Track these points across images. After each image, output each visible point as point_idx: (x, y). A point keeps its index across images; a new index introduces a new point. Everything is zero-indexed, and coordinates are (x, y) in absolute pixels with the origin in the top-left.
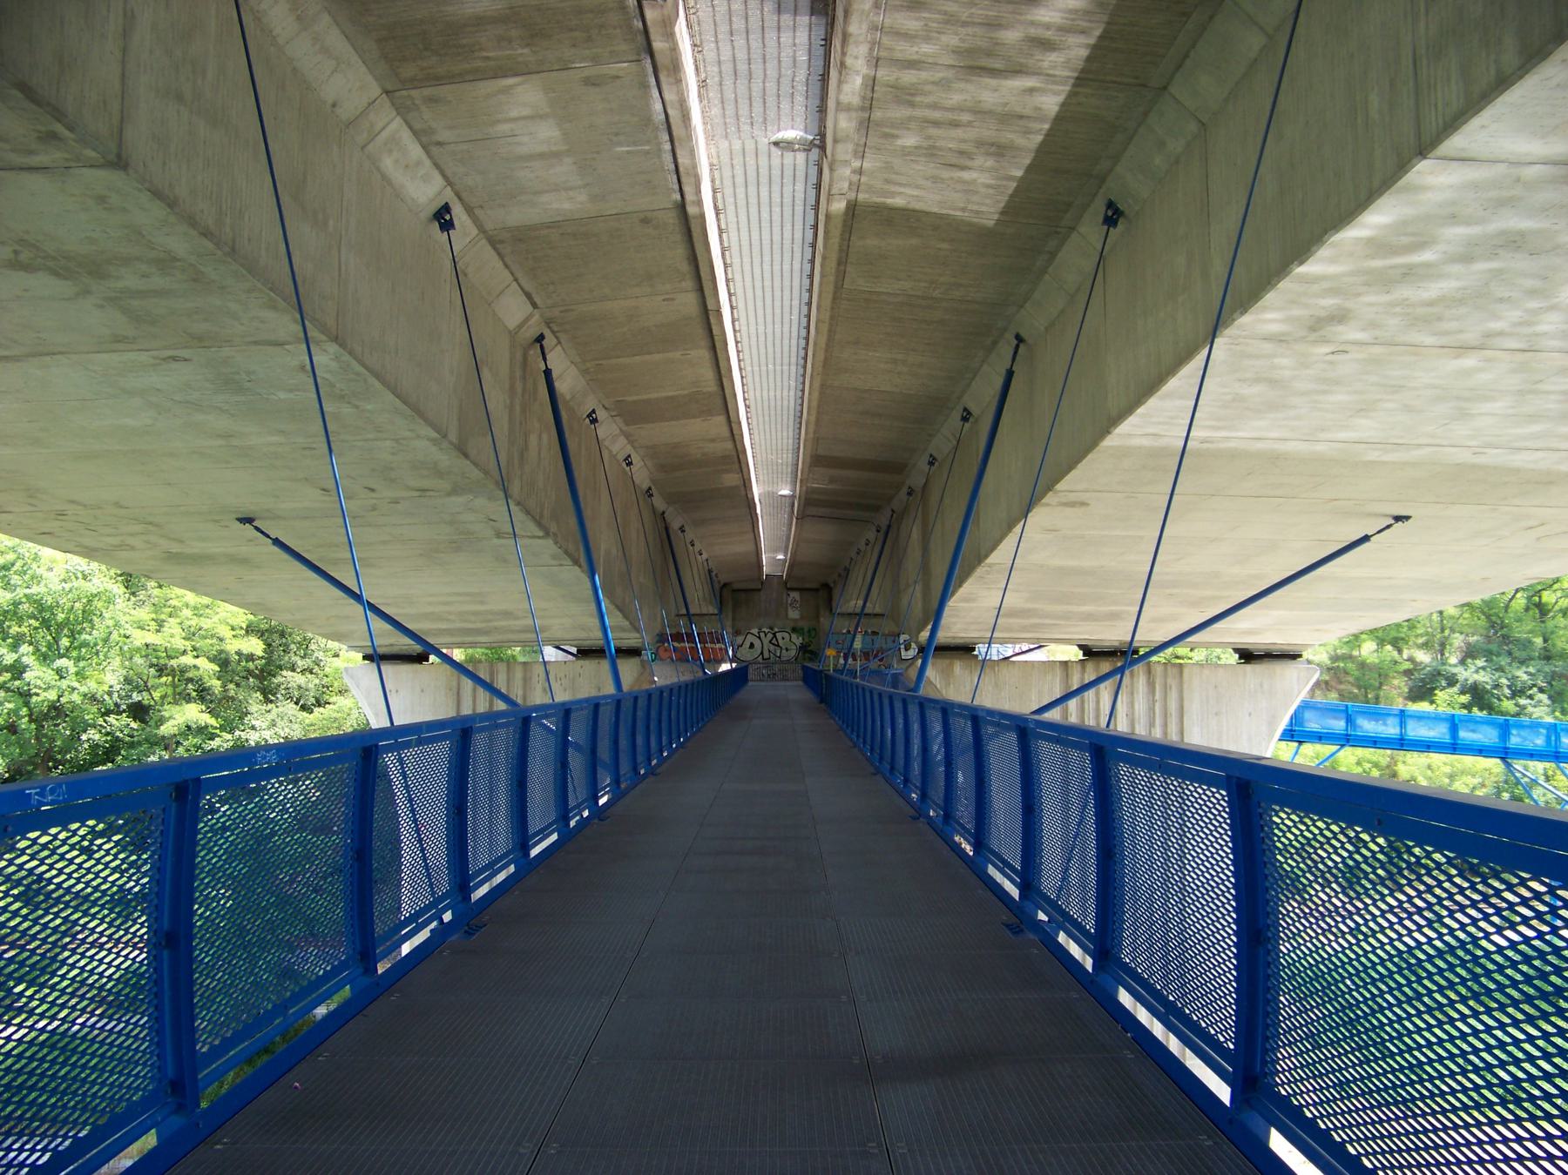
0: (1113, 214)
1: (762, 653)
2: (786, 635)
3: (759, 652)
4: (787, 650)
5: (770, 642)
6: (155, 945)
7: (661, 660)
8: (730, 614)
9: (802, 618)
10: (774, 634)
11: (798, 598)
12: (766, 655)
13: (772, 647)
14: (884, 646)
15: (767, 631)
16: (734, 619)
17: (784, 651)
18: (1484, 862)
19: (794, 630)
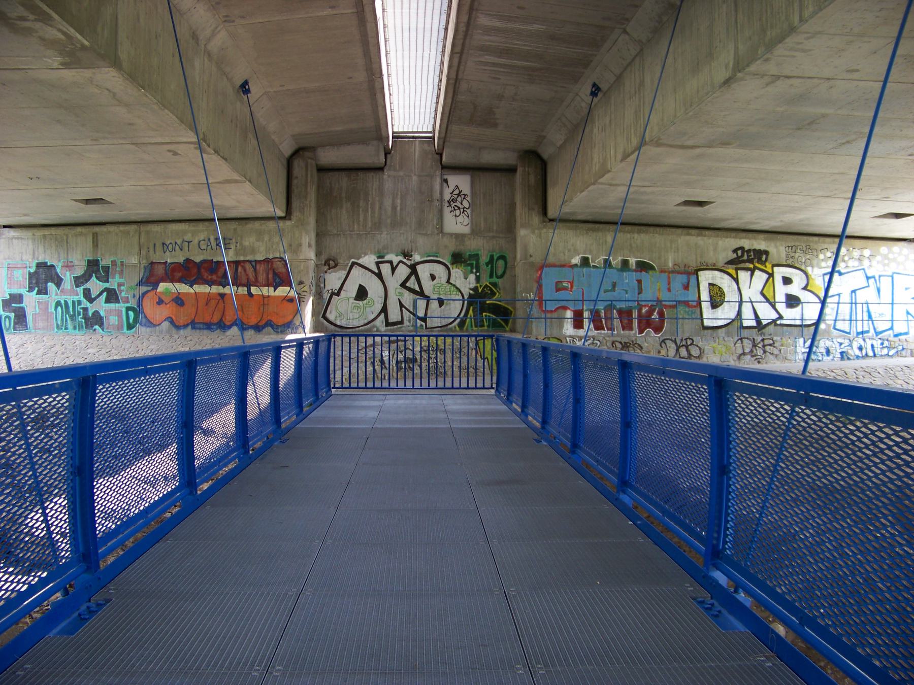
0: (595, 90)
1: (384, 310)
2: (440, 270)
3: (379, 307)
4: (441, 302)
5: (403, 285)
6: (71, 473)
7: (150, 324)
8: (312, 220)
9: (475, 232)
10: (413, 269)
11: (466, 189)
12: (394, 316)
13: (408, 298)
14: (664, 296)
15: (396, 259)
16: (320, 236)
17: (434, 305)
18: (858, 419)
19: (457, 258)
